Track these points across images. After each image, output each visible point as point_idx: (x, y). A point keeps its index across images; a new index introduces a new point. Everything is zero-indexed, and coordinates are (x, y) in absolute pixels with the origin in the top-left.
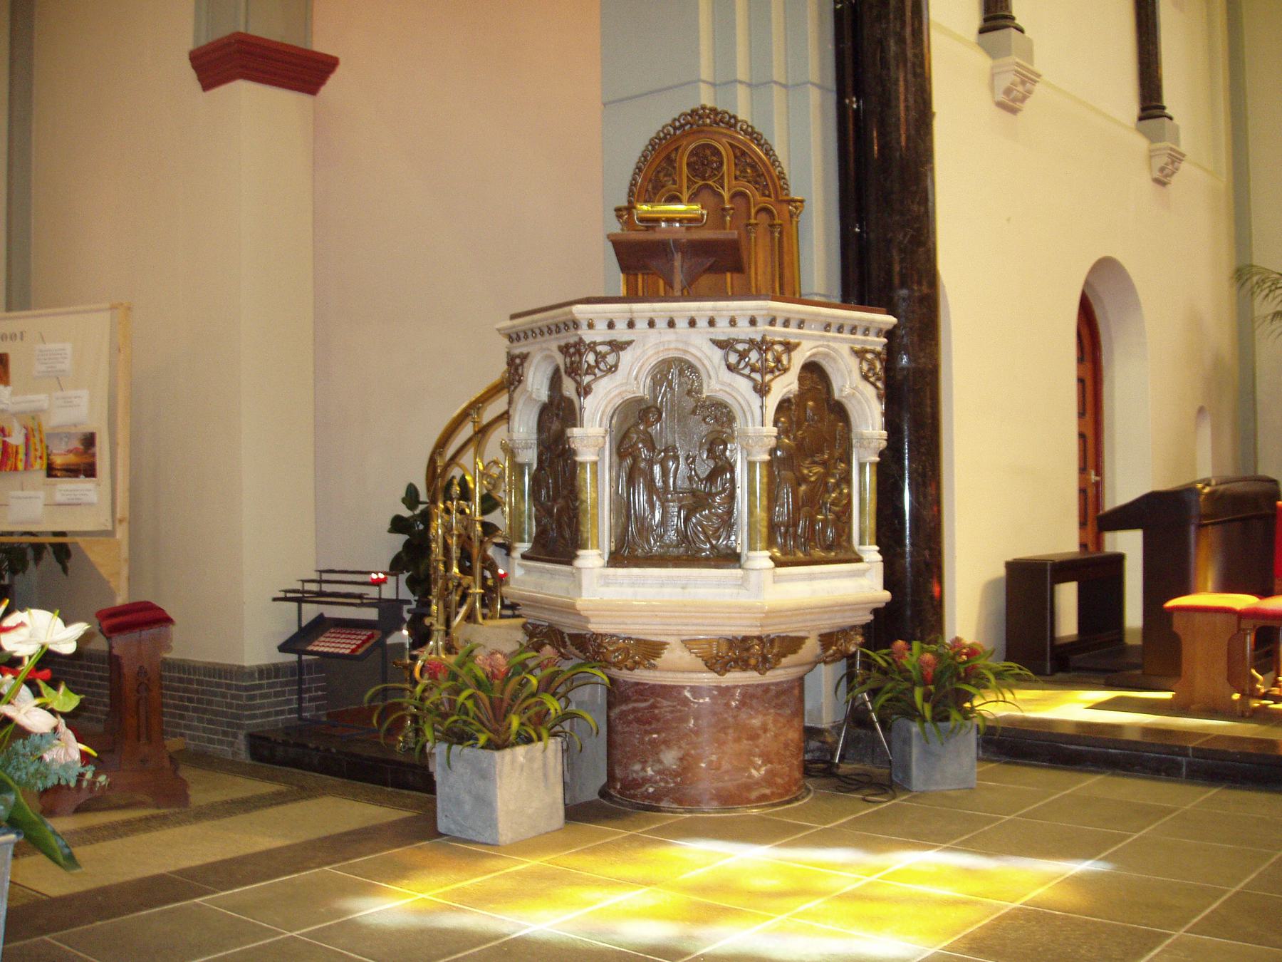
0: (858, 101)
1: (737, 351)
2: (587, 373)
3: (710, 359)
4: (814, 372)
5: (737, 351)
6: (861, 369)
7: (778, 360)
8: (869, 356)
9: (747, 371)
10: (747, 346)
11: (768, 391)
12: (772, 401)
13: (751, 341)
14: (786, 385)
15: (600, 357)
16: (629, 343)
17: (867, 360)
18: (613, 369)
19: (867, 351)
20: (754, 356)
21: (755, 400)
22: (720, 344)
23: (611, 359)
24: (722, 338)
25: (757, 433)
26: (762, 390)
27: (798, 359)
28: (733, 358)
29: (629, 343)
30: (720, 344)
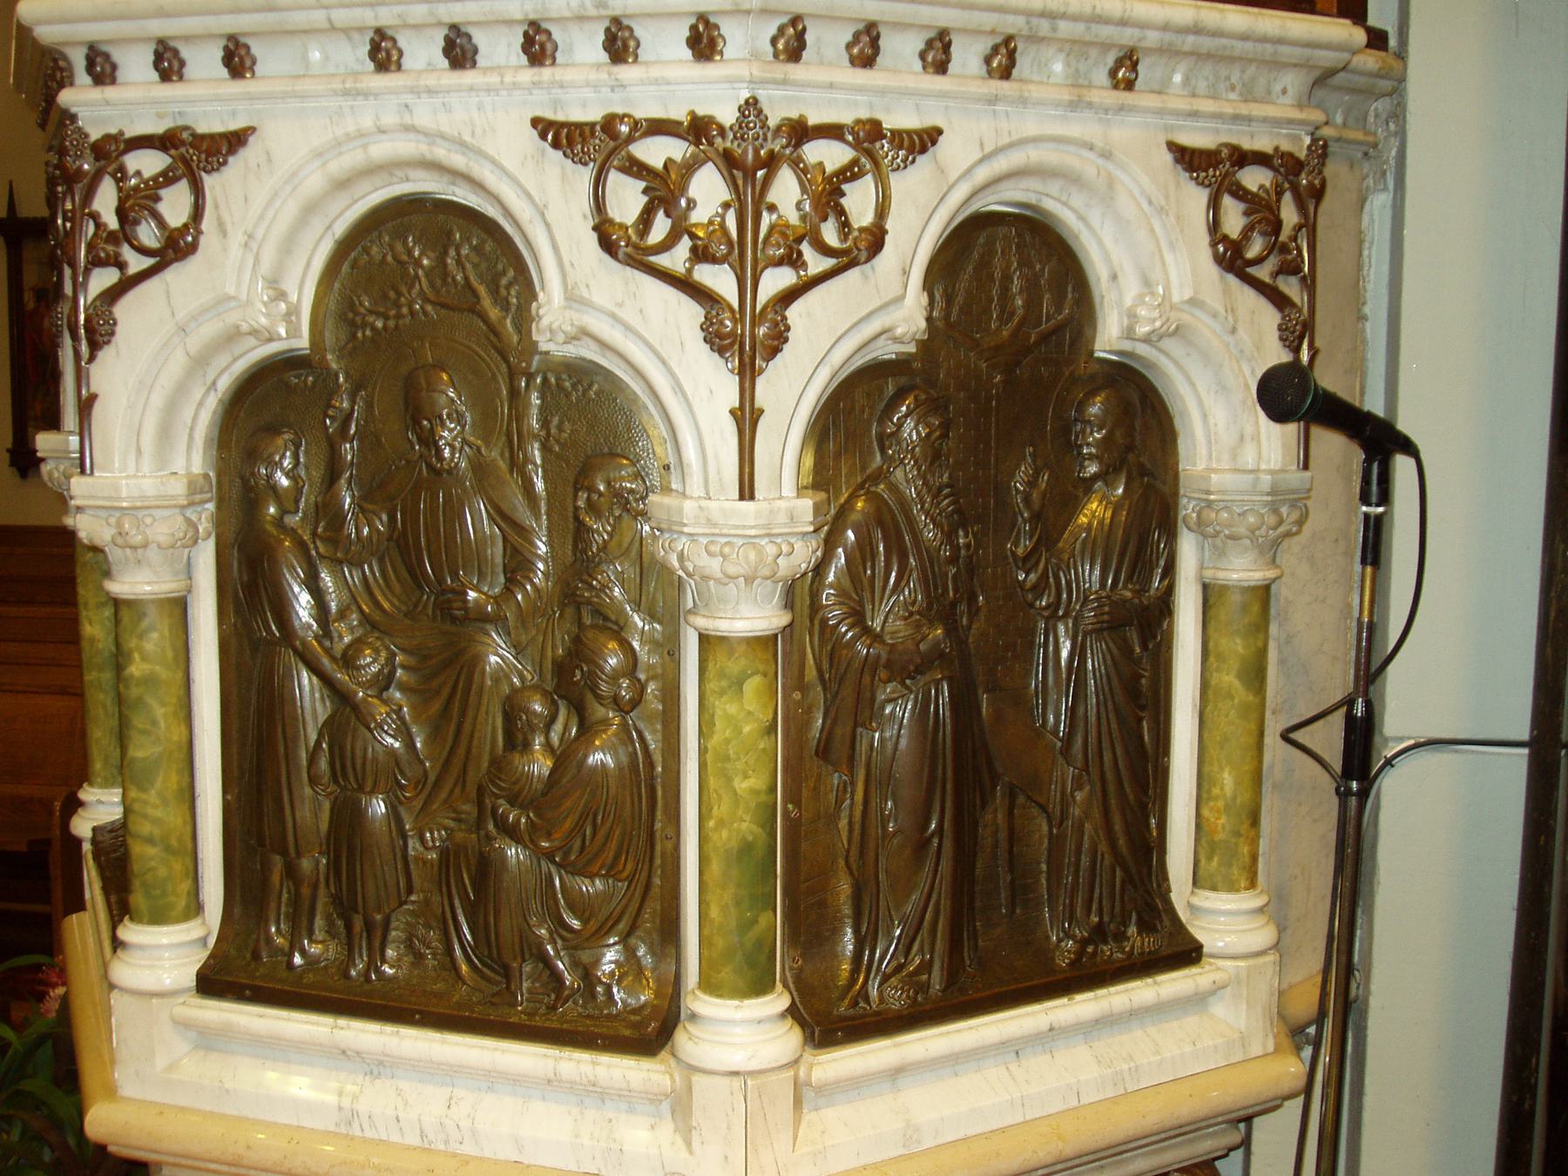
0: (966, 536)
1: (636, 168)
2: (96, 262)
3: (550, 209)
4: (1011, 269)
5: (636, 168)
6: (1214, 226)
7: (827, 195)
8: (1254, 179)
9: (677, 259)
10: (1227, 201)
11: (778, 340)
12: (795, 387)
13: (698, 129)
14: (873, 310)
15: (138, 202)
16: (236, 140)
17: (1240, 193)
18: (176, 247)
19: (1242, 158)
20: (708, 192)
21: (709, 385)
22: (561, 136)
23: (175, 206)
24: (588, 112)
25: (735, 519)
26: (748, 343)
27: (918, 212)
28: (626, 199)
29: (236, 140)
30: (561, 136)
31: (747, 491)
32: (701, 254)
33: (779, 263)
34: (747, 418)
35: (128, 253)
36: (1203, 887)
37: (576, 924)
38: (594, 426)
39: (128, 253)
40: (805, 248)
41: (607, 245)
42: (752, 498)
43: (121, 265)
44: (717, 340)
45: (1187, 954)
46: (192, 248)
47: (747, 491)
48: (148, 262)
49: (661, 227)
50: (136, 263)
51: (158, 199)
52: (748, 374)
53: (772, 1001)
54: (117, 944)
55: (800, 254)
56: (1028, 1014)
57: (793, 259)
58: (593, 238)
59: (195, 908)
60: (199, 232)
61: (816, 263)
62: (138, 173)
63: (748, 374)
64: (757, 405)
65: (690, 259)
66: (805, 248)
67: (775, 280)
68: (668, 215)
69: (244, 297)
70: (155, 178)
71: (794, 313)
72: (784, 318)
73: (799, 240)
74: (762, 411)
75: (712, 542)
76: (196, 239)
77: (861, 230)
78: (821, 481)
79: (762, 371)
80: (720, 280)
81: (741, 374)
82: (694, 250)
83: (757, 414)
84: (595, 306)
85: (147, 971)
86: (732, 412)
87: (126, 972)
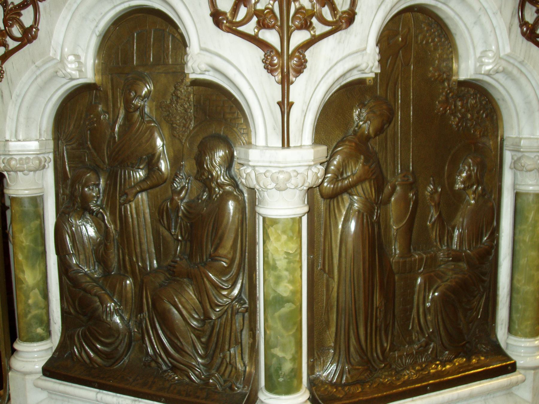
12: (311, 92)
14: (349, 55)
26: (286, 67)
31: (286, 143)
32: (262, 25)
33: (300, 28)
34: (285, 105)
35: (9, 40)
36: (516, 335)
37: (424, 42)
38: (217, 114)
39: (9, 40)
40: (314, 20)
41: (218, 23)
42: (288, 146)
43: (5, 45)
44: (270, 68)
45: (511, 368)
46: (35, 37)
47: (286, 143)
48: (16, 44)
49: (243, 11)
50: (12, 44)
51: (20, 15)
52: (285, 83)
53: (301, 396)
54: (14, 351)
55: (311, 23)
56: (428, 397)
57: (306, 26)
58: (210, 20)
59: (49, 334)
60: (38, 30)
61: (320, 29)
62: (12, 3)
63: (285, 83)
64: (290, 100)
65: (256, 27)
66: (314, 20)
67: (299, 37)
68: (245, 6)
69: (59, 58)
70: (19, 5)
71: (308, 54)
72: (304, 56)
73: (312, 16)
74: (292, 104)
75: (267, 171)
76: (36, 33)
77: (344, 12)
78: (319, 137)
79: (292, 83)
80: (271, 37)
81: (282, 83)
82: (258, 22)
83: (290, 105)
84: (217, 56)
85: (31, 357)
86: (279, 103)
87: (17, 363)
